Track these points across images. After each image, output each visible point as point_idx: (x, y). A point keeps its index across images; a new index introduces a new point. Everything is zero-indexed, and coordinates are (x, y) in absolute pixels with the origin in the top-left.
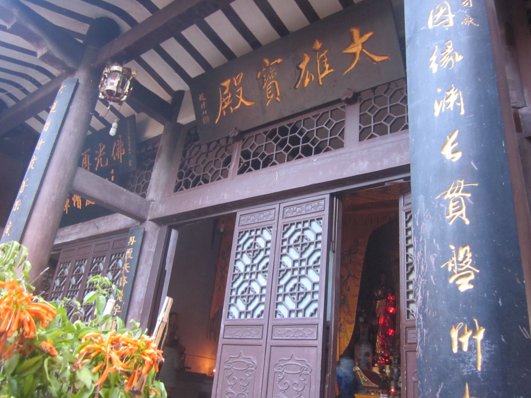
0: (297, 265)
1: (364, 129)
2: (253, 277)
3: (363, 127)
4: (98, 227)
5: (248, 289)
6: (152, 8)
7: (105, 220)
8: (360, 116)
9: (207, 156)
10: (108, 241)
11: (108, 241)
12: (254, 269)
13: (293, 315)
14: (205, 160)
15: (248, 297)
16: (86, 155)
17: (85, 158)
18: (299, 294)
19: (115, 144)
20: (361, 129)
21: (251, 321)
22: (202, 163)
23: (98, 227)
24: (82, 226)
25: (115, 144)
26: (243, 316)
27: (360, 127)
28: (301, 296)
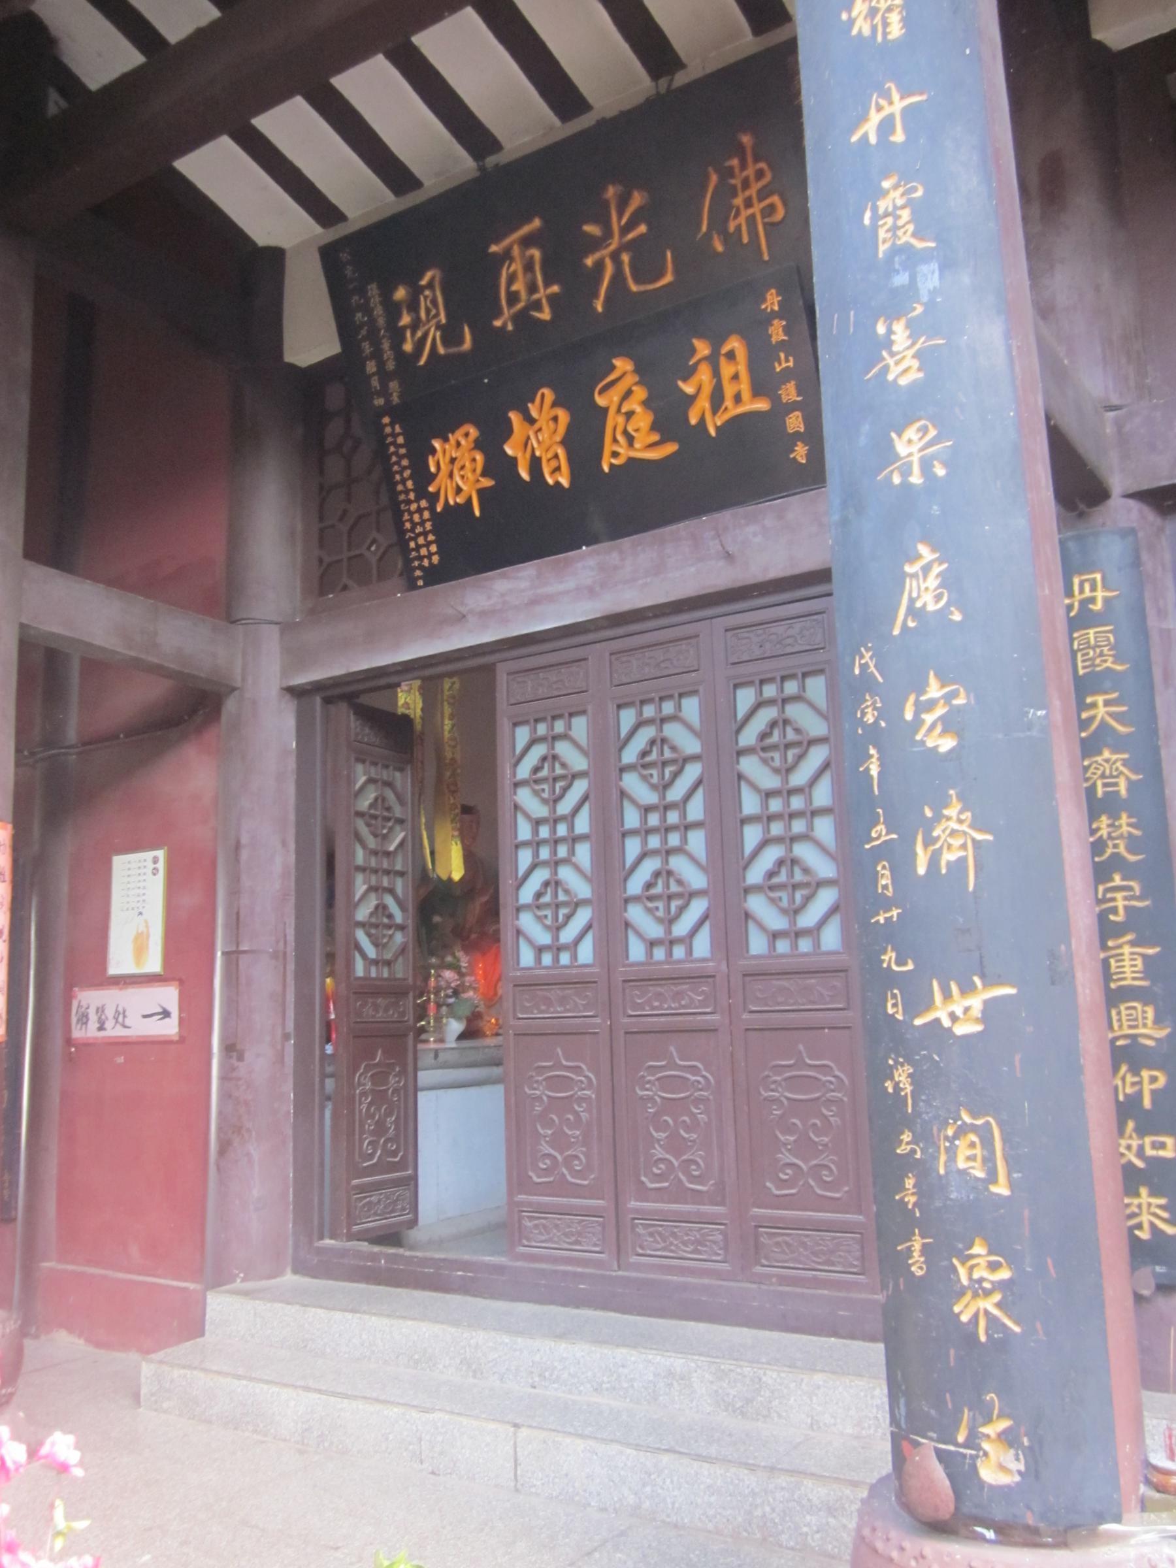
0: (544, 832)
1: (330, 565)
2: (562, 851)
3: (327, 560)
4: (729, 557)
5: (553, 884)
6: (138, 30)
7: (769, 521)
8: (322, 530)
9: (349, 497)
10: (688, 629)
11: (688, 629)
12: (562, 830)
13: (547, 959)
14: (345, 512)
15: (555, 905)
16: (516, 251)
17: (517, 266)
18: (558, 906)
19: (714, 178)
20: (325, 565)
21: (537, 972)
22: (341, 519)
23: (729, 557)
24: (614, 558)
25: (714, 178)
26: (547, 959)
27: (321, 561)
28: (563, 911)
